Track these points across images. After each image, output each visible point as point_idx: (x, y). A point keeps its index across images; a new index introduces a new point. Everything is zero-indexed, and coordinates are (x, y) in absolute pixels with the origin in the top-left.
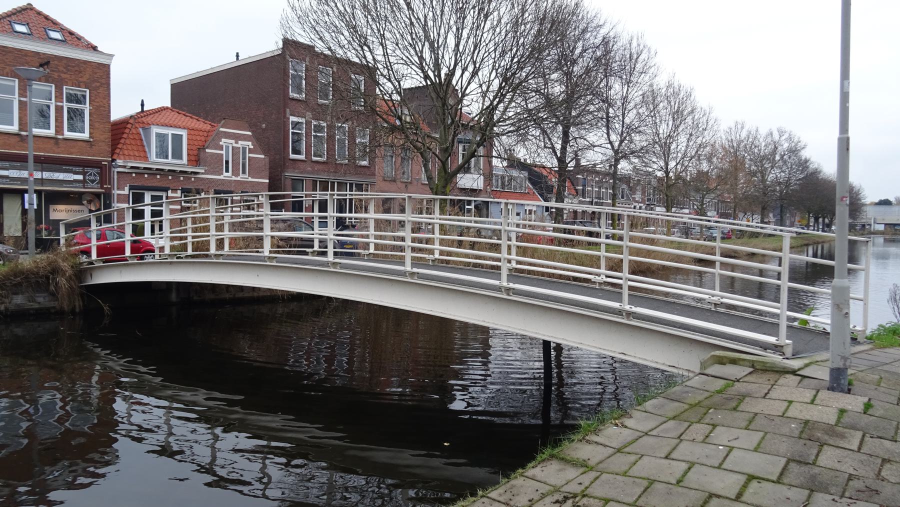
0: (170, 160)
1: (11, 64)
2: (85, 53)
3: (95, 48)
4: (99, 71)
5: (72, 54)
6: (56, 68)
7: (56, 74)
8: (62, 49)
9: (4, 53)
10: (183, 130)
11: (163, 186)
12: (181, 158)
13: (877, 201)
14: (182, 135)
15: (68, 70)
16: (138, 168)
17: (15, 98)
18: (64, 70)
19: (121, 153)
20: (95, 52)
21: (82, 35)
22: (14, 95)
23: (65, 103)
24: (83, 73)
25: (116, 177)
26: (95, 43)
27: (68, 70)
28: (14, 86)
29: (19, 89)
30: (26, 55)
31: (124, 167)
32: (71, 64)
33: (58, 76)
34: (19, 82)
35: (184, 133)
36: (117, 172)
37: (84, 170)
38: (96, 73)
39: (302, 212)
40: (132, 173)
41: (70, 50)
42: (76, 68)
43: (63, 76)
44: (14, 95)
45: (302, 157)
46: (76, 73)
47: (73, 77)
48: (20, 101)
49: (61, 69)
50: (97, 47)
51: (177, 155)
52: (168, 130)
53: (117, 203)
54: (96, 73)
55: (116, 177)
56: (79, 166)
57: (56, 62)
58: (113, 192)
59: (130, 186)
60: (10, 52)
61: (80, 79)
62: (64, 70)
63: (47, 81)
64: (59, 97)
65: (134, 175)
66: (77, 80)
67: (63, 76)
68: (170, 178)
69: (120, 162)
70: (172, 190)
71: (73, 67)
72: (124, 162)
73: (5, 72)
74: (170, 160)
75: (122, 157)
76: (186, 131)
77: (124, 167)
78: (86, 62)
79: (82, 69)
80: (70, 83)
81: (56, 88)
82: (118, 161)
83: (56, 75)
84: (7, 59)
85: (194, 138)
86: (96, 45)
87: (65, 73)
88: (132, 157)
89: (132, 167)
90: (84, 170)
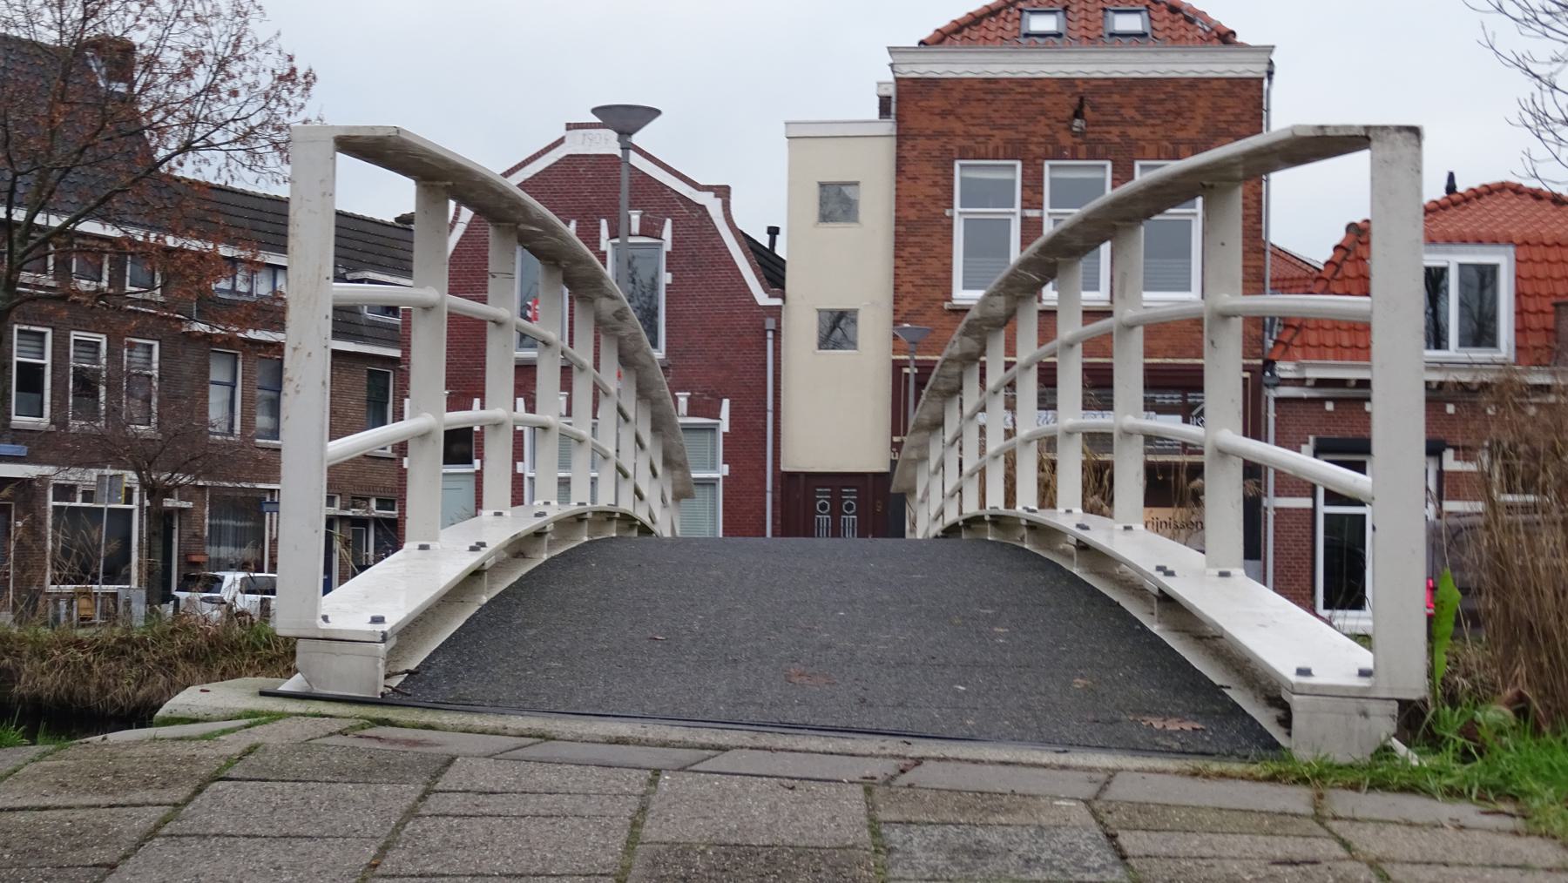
0: (1454, 351)
1: (1006, 122)
2: (1192, 57)
3: (1226, 37)
4: (1230, 102)
5: (1212, 67)
6: (1117, 113)
7: (1115, 130)
8: (1075, 56)
9: (989, 97)
10: (1501, 249)
11: (1350, 435)
12: (1493, 343)
13: (927, 33)
14: (965, 288)
15: (1147, 114)
16: (1341, 383)
17: (1195, 214)
18: (1138, 117)
19: (1296, 341)
20: (1227, 48)
21: (1199, 6)
22: (1013, 206)
23: (1047, 208)
24: (1188, 114)
25: (1272, 415)
26: (1229, 25)
27: (1147, 114)
28: (1013, 182)
29: (1024, 186)
30: (1042, 93)
31: (1301, 382)
32: (1155, 97)
33: (1123, 134)
34: (1024, 167)
35: (1503, 259)
36: (1278, 400)
37: (1185, 398)
38: (1222, 110)
39: (263, 572)
40: (1322, 401)
41: (1154, 57)
42: (1170, 106)
43: (1134, 132)
44: (1013, 206)
45: (74, 335)
46: (1170, 118)
47: (1160, 131)
48: (1024, 219)
49: (1129, 113)
50: (1233, 33)
51: (1481, 332)
52: (1449, 252)
53: (1277, 494)
54: (1222, 110)
55: (1272, 415)
56: (1175, 388)
57: (1116, 98)
58: (1265, 502)
59: (1318, 440)
60: (1004, 92)
61: (1180, 135)
62: (1138, 117)
63: (1092, 155)
64: (1032, 198)
65: (1329, 406)
66: (1168, 138)
67: (1134, 132)
68: (1450, 409)
69: (1285, 369)
70: (1456, 448)
71: (1161, 102)
72: (1301, 367)
73: (991, 146)
74: (1454, 351)
75: (1297, 353)
76: (1511, 250)
77: (1301, 382)
78: (1195, 84)
79: (1184, 103)
80: (1151, 149)
81: (1114, 172)
82: (1280, 365)
83: (1114, 134)
84: (996, 111)
85: (1541, 271)
86: (1230, 27)
87: (1138, 124)
88: (1330, 352)
89: (1321, 383)
90: (1185, 398)
